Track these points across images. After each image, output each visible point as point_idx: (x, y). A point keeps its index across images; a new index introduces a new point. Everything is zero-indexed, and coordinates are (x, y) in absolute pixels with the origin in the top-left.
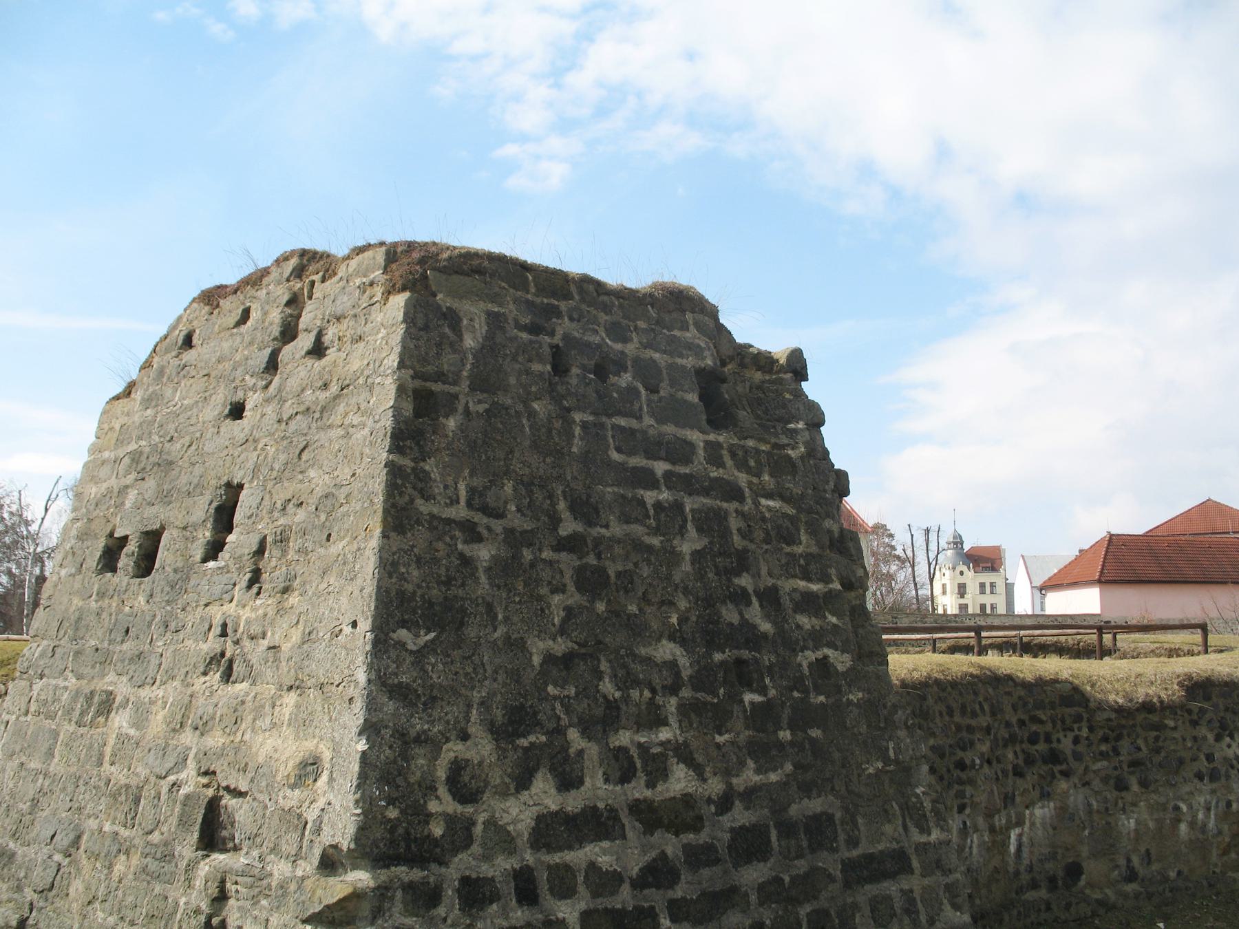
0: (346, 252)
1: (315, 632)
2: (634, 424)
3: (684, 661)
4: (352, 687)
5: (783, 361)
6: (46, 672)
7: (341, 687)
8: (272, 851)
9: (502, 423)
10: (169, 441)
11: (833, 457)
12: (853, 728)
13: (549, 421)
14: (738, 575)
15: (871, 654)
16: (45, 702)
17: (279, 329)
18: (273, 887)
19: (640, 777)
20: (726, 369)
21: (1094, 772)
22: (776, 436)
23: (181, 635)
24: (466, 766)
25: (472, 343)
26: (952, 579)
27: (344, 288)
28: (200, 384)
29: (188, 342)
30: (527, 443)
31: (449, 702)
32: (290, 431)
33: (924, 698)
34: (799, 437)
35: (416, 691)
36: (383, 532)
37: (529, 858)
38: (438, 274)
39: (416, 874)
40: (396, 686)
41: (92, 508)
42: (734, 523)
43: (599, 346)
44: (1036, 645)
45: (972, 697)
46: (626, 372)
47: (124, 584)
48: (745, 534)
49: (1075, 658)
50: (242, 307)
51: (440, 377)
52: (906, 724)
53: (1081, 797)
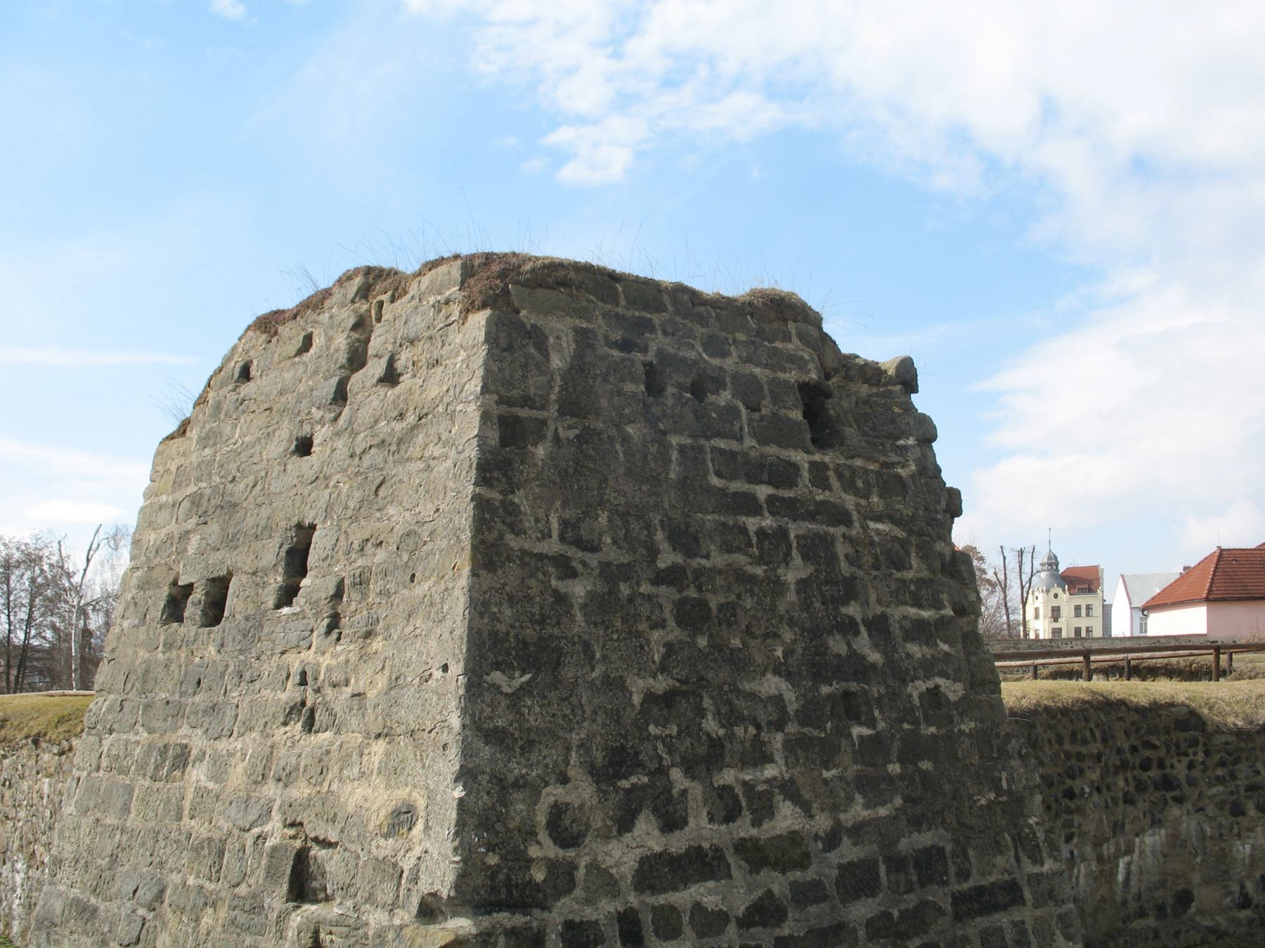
0: (417, 267)
1: (402, 677)
2: (733, 445)
3: (790, 695)
4: (446, 733)
5: (891, 372)
6: (116, 726)
7: (433, 734)
8: (367, 900)
9: (593, 449)
10: (231, 482)
11: (945, 476)
12: (965, 758)
13: (645, 446)
14: (846, 603)
15: (983, 683)
16: (117, 757)
17: (346, 356)
18: (370, 937)
19: (745, 816)
20: (830, 383)
21: (1209, 797)
22: (886, 455)
23: (257, 685)
24: (567, 810)
25: (560, 364)
26: (1046, 602)
27: (416, 308)
28: (261, 419)
29: (245, 374)
30: (622, 470)
31: (547, 745)
32: (364, 466)
33: (1033, 726)
34: (909, 454)
35: (513, 735)
36: (472, 570)
37: (633, 900)
38: (519, 288)
39: (519, 920)
40: (492, 730)
41: (152, 556)
42: (841, 549)
43: (695, 362)
44: (1144, 668)
45: (1084, 723)
46: (725, 389)
47: (193, 634)
48: (853, 560)
49: (1186, 681)
50: (303, 334)
51: (527, 401)
52: (1019, 753)
53: (1193, 823)
